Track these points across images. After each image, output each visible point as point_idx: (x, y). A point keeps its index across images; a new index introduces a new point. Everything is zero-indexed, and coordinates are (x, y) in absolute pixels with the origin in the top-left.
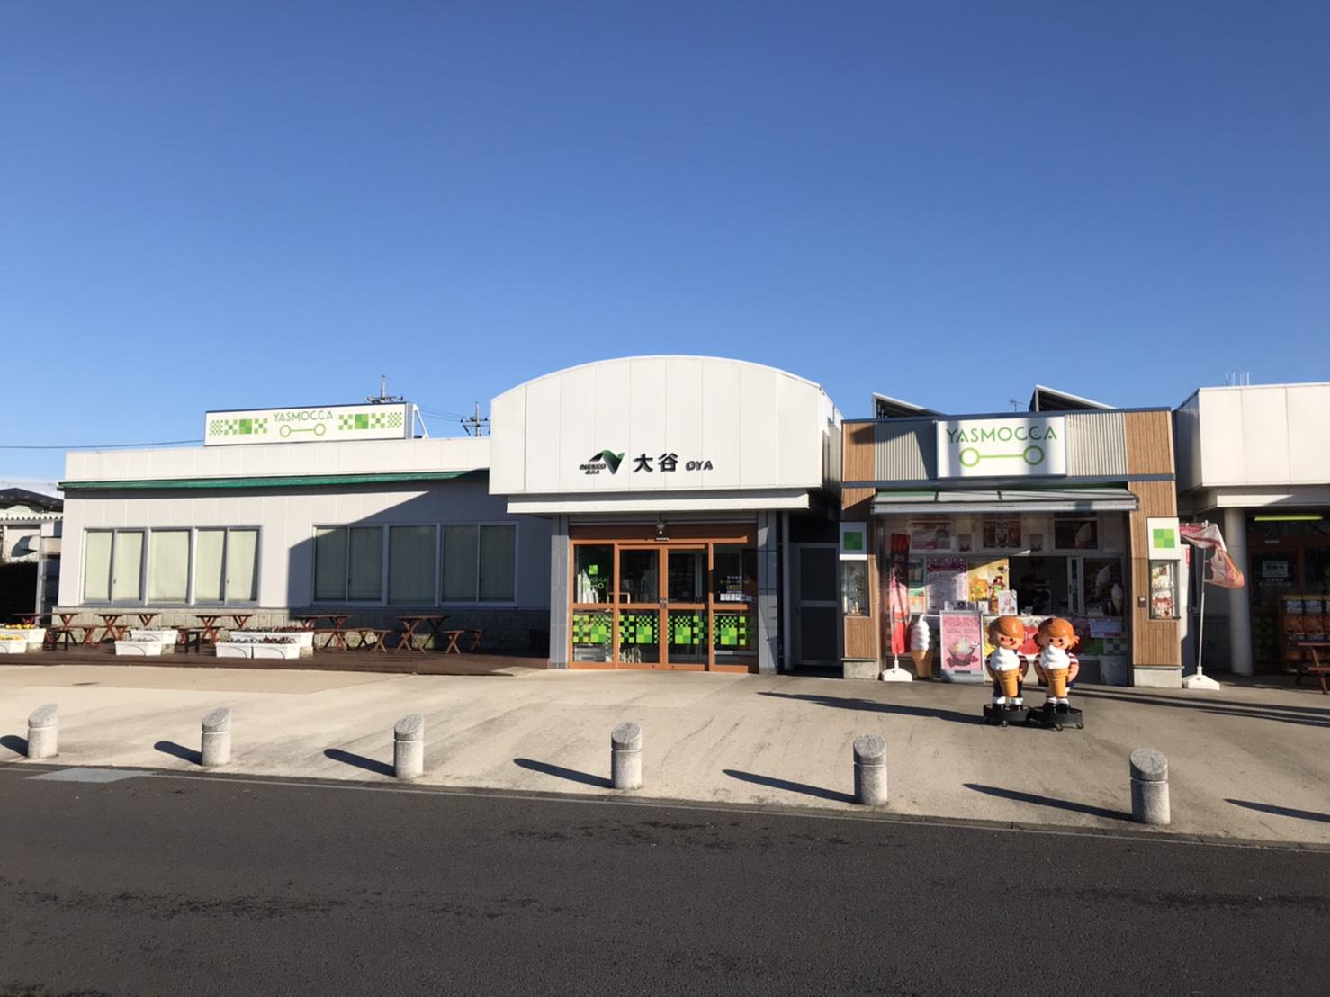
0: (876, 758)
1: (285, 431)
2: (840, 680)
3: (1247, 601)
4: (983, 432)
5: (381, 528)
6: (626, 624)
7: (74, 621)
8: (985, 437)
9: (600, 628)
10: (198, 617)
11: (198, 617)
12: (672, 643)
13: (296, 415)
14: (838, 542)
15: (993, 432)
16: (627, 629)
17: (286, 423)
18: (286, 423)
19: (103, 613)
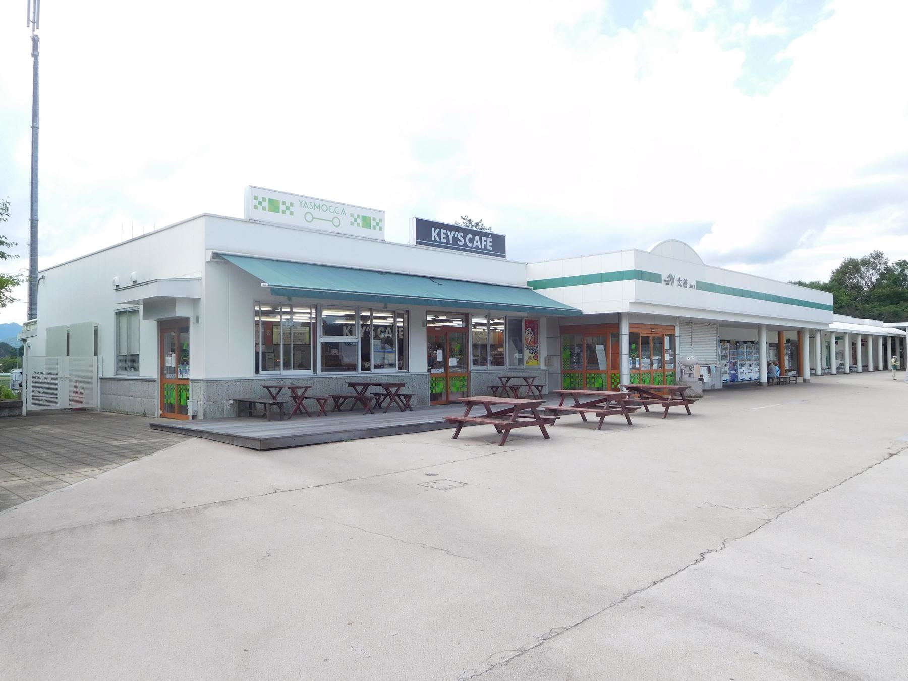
0: (499, 336)
1: (309, 217)
2: (697, 280)
3: (804, 355)
4: (315, 205)
5: (362, 370)
6: (616, 383)
7: (309, 393)
8: (316, 209)
9: (599, 380)
10: (264, 387)
11: (264, 387)
12: (432, 394)
13: (317, 205)
14: (293, 344)
15: (319, 205)
16: (616, 381)
17: (309, 210)
18: (309, 210)
19: (266, 385)
